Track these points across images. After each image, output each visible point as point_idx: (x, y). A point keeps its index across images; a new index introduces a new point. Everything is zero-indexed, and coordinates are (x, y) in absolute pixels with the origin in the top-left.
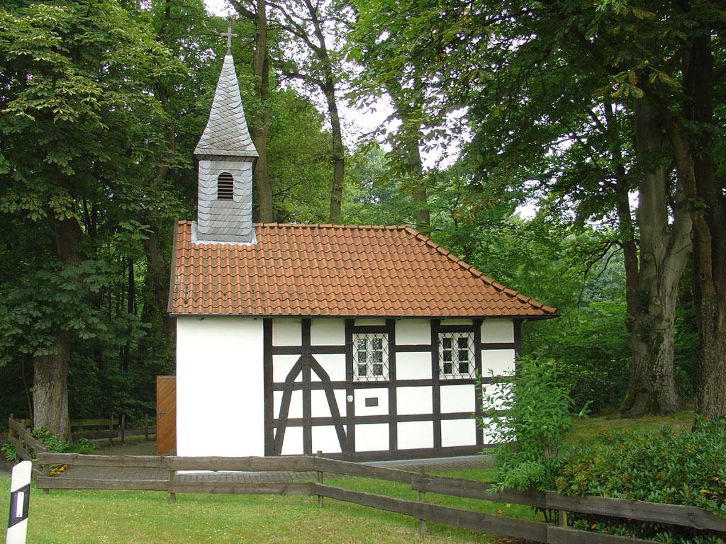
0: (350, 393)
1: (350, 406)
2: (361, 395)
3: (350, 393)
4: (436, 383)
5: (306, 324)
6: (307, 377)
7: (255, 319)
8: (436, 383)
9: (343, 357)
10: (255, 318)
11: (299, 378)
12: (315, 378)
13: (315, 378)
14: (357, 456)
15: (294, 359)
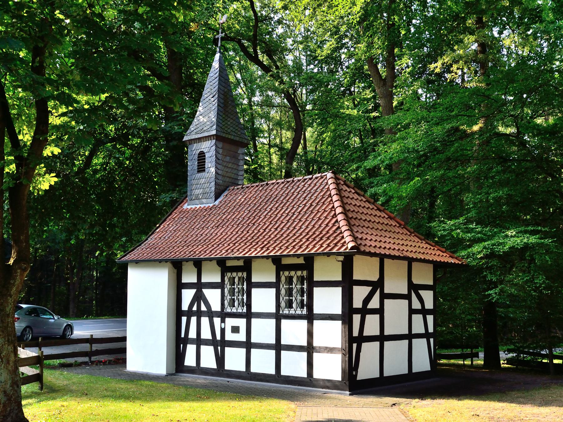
0: (223, 321)
1: (223, 331)
2: (230, 322)
3: (223, 321)
4: (278, 317)
5: (198, 264)
6: (199, 307)
7: (160, 262)
8: (278, 317)
9: (273, 291)
10: (166, 261)
11: (195, 308)
12: (203, 308)
13: (203, 308)
14: (225, 372)
15: (193, 291)
